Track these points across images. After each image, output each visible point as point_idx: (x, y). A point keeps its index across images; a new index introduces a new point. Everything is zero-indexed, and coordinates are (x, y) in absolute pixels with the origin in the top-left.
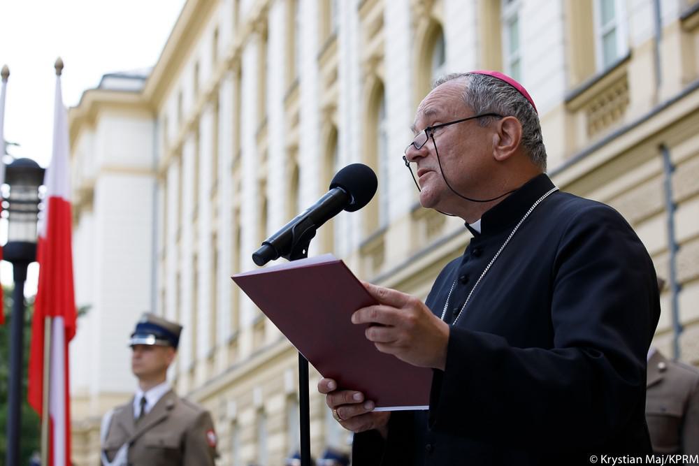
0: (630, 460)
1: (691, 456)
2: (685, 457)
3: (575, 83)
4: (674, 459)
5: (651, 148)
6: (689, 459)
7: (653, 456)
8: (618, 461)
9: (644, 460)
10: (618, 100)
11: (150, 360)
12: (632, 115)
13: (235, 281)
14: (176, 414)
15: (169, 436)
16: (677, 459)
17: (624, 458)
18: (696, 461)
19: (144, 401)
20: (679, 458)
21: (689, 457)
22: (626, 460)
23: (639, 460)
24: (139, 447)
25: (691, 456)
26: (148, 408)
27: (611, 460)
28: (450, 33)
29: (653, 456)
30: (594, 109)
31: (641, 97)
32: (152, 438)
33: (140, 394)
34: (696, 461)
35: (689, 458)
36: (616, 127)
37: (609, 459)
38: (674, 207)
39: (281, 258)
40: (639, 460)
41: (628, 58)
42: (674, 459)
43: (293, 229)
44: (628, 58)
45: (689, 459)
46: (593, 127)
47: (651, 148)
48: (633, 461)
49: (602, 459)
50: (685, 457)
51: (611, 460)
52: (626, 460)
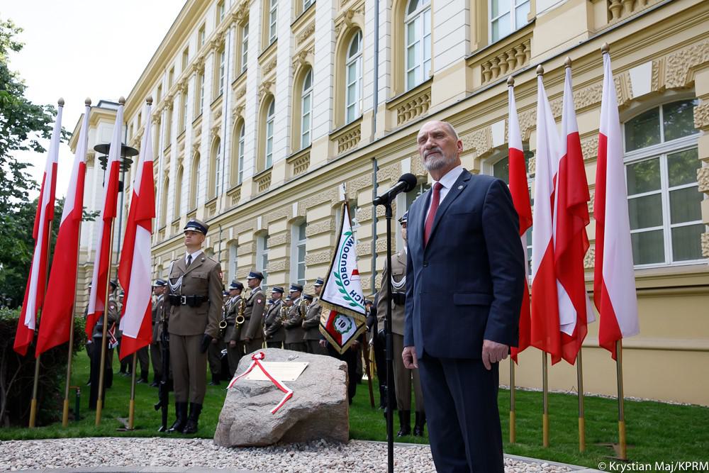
0: (639, 466)
1: (701, 463)
2: (695, 464)
3: (475, 48)
4: (684, 466)
5: (369, 159)
6: (698, 466)
7: (662, 463)
8: (626, 467)
9: (653, 466)
10: (306, 162)
11: (195, 238)
12: (360, 145)
13: (128, 356)
14: (205, 264)
15: (203, 273)
16: (687, 466)
17: (633, 465)
18: (706, 468)
19: (190, 257)
20: (688, 464)
21: (699, 463)
22: (635, 467)
23: (648, 467)
24: (189, 278)
25: (701, 463)
26: (192, 261)
27: (620, 467)
28: (315, 69)
29: (662, 463)
30: (234, 197)
31: (365, 138)
32: (195, 274)
33: (188, 254)
34: (706, 468)
35: (699, 465)
36: (304, 172)
37: (617, 466)
38: (377, 185)
39: (541, 351)
40: (648, 467)
41: (361, 118)
42: (684, 466)
43: (43, 366)
44: (361, 118)
45: (698, 466)
46: (296, 170)
47: (369, 159)
48: (642, 467)
49: (611, 466)
50: (695, 464)
51: (620, 467)
52: (635, 467)
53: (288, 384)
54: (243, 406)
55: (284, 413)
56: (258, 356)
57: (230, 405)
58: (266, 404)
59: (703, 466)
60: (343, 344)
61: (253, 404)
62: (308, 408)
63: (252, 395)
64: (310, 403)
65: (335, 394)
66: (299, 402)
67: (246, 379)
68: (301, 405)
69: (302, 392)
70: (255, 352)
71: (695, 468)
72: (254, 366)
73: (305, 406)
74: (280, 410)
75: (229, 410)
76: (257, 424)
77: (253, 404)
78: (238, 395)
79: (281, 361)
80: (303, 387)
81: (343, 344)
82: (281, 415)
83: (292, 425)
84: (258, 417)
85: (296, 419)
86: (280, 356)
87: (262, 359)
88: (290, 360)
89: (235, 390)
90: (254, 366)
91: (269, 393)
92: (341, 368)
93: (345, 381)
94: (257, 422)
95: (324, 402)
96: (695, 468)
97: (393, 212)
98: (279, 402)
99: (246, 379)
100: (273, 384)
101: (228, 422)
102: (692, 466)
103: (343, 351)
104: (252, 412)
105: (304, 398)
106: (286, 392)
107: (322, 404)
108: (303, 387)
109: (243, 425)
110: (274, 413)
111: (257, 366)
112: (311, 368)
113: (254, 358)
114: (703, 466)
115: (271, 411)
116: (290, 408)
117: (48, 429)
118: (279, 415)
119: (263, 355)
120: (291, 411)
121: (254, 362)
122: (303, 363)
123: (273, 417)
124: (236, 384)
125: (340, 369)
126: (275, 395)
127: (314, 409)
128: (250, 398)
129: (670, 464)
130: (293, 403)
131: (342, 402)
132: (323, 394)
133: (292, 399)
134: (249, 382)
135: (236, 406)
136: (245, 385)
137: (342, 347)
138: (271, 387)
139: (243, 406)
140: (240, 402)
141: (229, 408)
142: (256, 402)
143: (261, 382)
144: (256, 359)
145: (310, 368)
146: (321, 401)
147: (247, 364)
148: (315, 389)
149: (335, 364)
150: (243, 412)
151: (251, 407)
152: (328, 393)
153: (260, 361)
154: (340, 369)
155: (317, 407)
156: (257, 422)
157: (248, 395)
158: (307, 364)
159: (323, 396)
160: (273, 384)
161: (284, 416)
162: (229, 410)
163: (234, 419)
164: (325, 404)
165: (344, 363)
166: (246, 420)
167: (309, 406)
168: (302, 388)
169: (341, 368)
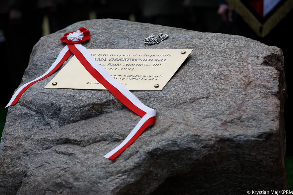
0: (264, 192)
1: (290, 191)
2: (287, 191)
4: (283, 192)
6: (289, 192)
7: (274, 191)
8: (259, 193)
9: (270, 193)
16: (284, 192)
17: (262, 192)
18: (292, 193)
20: (284, 191)
22: (262, 193)
23: (268, 192)
25: (290, 191)
27: (256, 192)
29: (274, 191)
34: (292, 193)
35: (289, 192)
37: (255, 192)
40: (268, 192)
42: (283, 192)
45: (289, 192)
48: (265, 193)
49: (252, 192)
50: (287, 191)
52: (262, 193)
53: (143, 95)
54: (45, 144)
55: (136, 159)
56: (76, 35)
57: (14, 144)
58: (95, 141)
59: (291, 192)
60: (267, 10)
61: (67, 141)
62: (190, 150)
63: (64, 122)
64: (196, 138)
65: (253, 118)
66: (170, 135)
67: (49, 85)
68: (175, 143)
69: (176, 113)
70: (69, 28)
71: (287, 193)
72: (66, 58)
73: (184, 144)
74: (127, 152)
75: (13, 154)
76: (75, 183)
77: (67, 141)
78: (31, 122)
79: (129, 46)
80: (180, 103)
81: (267, 10)
82: (130, 163)
83: (155, 185)
84: (78, 168)
85: (163, 173)
86: (125, 37)
87: (85, 42)
88: (150, 44)
89: (24, 110)
90: (66, 58)
91: (104, 116)
92: (268, 61)
93: (276, 89)
94: (77, 179)
95: (227, 134)
96: (287, 193)
97: (69, 60)
98: (124, 137)
99: (49, 85)
100: (112, 97)
101: (10, 180)
102: (286, 192)
103: (267, 28)
104: (64, 158)
105: (182, 126)
106: (142, 114)
107: (222, 140)
108: (180, 103)
109: (45, 186)
110: (114, 159)
111: (74, 60)
112: (198, 61)
113: (65, 42)
114: (291, 192)
115: (108, 155)
116: (151, 148)
117: (199, 136)
118: (122, 164)
119: (86, 33)
120: (153, 155)
121: (66, 49)
122: (182, 50)
123: (112, 168)
124: (28, 96)
125: (265, 63)
126: (114, 121)
127: (205, 152)
128: (58, 129)
129: (277, 191)
130: (159, 138)
131: (268, 136)
132: (224, 118)
133: (156, 129)
134: (58, 92)
135: (27, 145)
136: (48, 99)
137: (263, 19)
138: (107, 104)
139: (45, 144)
140: (37, 137)
141: (12, 149)
142: (73, 137)
143: (83, 93)
144: (71, 43)
145: (199, 60)
146: (219, 133)
147: (50, 53)
148: (207, 107)
149: (254, 52)
150: (45, 158)
151: (63, 148)
152: (236, 115)
153: (79, 47)
154: (265, 63)
155: (212, 147)
156: (77, 179)
157: (54, 122)
158: (189, 52)
159: (225, 123)
160: (112, 97)
161: (138, 166)
162: (13, 154)
163: (25, 174)
164: (228, 140)
165: (276, 50)
166: (51, 177)
167: (194, 145)
168: (176, 105)
169: (268, 61)
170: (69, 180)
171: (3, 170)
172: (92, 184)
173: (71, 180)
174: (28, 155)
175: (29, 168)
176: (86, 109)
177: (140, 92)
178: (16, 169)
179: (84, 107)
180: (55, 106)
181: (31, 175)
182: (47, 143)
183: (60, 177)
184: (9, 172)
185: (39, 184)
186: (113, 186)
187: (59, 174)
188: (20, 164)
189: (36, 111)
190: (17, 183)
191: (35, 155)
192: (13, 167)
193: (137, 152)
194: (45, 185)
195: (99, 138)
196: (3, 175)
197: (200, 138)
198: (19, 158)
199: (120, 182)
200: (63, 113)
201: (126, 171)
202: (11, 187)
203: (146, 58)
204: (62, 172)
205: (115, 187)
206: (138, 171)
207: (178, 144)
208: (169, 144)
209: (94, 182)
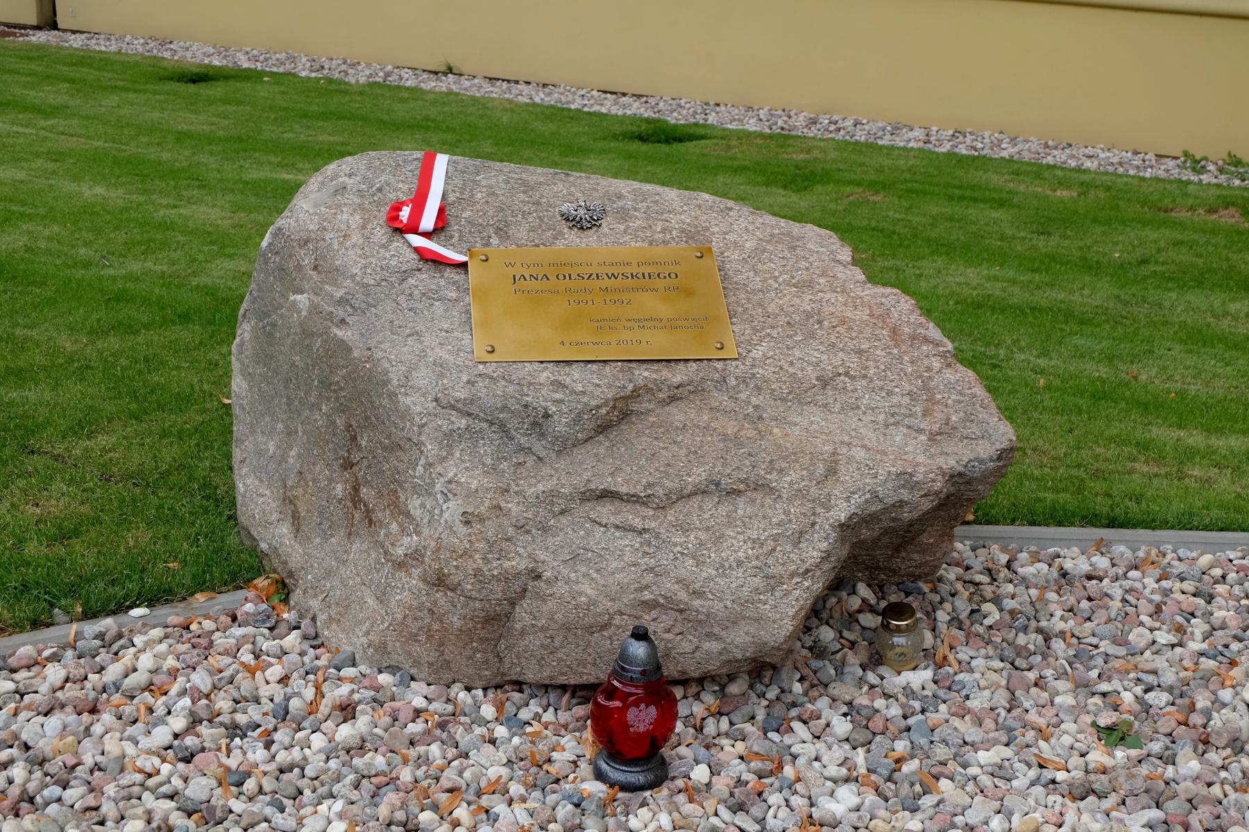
64: (906, 479)
94: (698, 594)
116: (841, 512)
117: (911, 475)
156: (698, 594)
167: (905, 495)
170: (676, 595)
171: (475, 566)
172: (742, 605)
173: (683, 595)
174: (528, 532)
175: (543, 563)
176: (603, 411)
177: (693, 366)
178: (507, 564)
179: (598, 407)
180: (534, 408)
181: (556, 578)
182: (560, 502)
183: (647, 587)
184: (490, 570)
185: (592, 603)
186: (793, 607)
187: (644, 582)
188: (517, 553)
189: (487, 421)
190: (515, 593)
191: (545, 529)
192: (499, 559)
193: (813, 524)
194: (609, 604)
195: (690, 487)
196: (475, 575)
197: (915, 479)
198: (508, 540)
199: (805, 596)
200: (560, 425)
201: (807, 571)
202: (500, 601)
203: (607, 283)
204: (650, 577)
205: (797, 608)
206: (826, 566)
207: (881, 496)
208: (867, 501)
209: (747, 601)
